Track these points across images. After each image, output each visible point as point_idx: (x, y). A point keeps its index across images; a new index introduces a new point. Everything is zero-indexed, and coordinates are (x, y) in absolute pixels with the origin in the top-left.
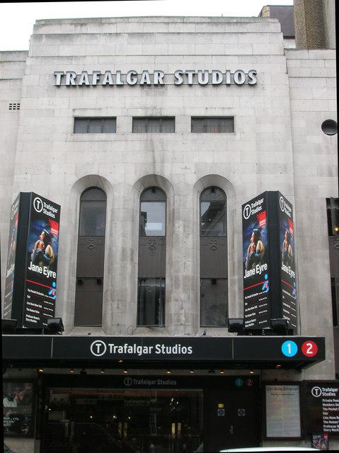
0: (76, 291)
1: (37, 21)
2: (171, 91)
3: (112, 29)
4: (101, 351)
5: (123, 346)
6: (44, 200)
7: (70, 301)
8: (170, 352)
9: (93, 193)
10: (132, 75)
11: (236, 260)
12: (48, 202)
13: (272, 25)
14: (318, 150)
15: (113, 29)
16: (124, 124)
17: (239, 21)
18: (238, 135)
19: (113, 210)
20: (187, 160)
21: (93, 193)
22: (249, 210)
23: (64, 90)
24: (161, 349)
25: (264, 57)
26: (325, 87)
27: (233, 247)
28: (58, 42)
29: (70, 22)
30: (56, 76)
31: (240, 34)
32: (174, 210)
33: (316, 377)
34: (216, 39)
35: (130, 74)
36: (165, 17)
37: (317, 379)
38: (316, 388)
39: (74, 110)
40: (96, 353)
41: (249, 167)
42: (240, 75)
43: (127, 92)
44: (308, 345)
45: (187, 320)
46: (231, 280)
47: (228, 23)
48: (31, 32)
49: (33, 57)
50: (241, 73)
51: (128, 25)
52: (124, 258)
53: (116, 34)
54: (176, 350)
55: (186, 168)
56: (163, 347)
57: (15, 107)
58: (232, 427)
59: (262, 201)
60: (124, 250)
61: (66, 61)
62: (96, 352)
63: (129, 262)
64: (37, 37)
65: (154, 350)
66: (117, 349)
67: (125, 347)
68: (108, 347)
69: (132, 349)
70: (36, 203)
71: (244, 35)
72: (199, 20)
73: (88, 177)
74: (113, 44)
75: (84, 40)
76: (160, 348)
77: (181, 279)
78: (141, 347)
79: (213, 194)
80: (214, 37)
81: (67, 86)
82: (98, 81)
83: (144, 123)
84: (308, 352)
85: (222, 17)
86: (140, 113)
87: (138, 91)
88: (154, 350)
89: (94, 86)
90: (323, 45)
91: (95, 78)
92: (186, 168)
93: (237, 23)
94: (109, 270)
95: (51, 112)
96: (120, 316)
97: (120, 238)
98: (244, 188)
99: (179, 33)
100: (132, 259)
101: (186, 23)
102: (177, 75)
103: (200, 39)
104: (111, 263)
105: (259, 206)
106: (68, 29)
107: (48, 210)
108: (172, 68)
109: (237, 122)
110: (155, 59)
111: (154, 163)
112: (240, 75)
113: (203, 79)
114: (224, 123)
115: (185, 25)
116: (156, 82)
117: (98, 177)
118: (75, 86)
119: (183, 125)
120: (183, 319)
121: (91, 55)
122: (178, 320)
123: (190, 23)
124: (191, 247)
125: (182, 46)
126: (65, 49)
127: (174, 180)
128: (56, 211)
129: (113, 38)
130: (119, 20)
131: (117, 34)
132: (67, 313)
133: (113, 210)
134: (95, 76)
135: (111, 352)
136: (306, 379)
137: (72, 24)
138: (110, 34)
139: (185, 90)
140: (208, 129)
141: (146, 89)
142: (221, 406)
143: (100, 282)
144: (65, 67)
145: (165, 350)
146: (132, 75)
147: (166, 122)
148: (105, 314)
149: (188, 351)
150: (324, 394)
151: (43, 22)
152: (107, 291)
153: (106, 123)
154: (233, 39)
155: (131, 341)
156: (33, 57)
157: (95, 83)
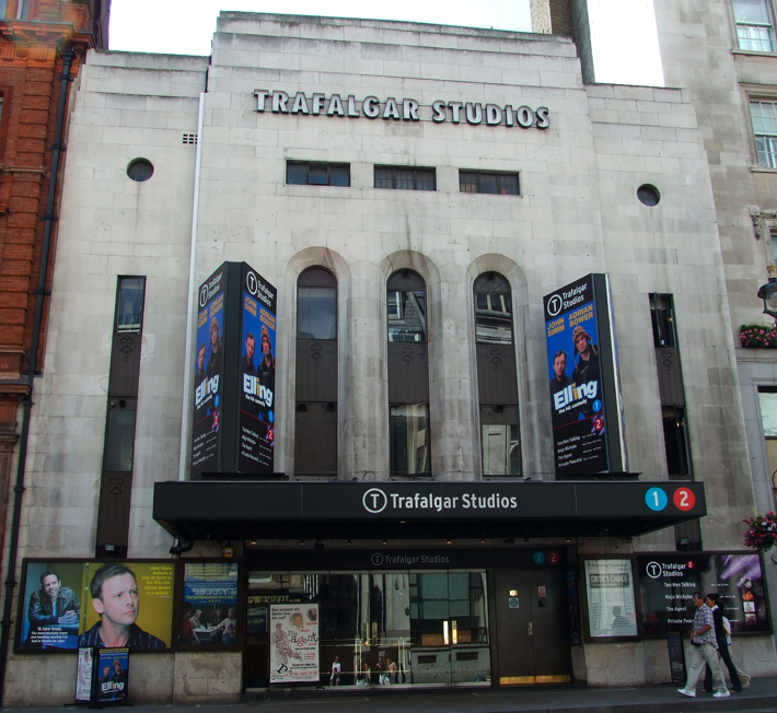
0: (297, 421)
1: (221, 13)
2: (429, 129)
3: (337, 35)
6: (259, 277)
7: (288, 436)
8: (484, 506)
9: (319, 277)
10: (372, 102)
11: (532, 378)
12: (264, 282)
13: (564, 46)
14: (634, 225)
15: (337, 35)
16: (362, 175)
17: (518, 37)
18: (526, 200)
19: (349, 301)
20: (455, 234)
21: (319, 277)
22: (558, 303)
23: (268, 118)
25: (558, 92)
26: (638, 138)
27: (526, 359)
28: (256, 46)
29: (273, 18)
30: (256, 96)
31: (521, 57)
32: (440, 303)
33: (650, 548)
35: (369, 101)
36: (413, 23)
37: (652, 550)
38: (653, 565)
39: (286, 149)
40: (372, 508)
41: (544, 244)
42: (525, 113)
44: (681, 493)
45: (466, 465)
47: (505, 40)
48: (214, 28)
49: (218, 66)
50: (284, 96)
51: (359, 29)
52: (370, 374)
53: (344, 42)
54: (492, 502)
55: (455, 242)
56: (474, 498)
57: (190, 140)
59: (584, 288)
60: (370, 361)
61: (270, 77)
63: (377, 378)
64: (222, 37)
65: (460, 502)
66: (404, 502)
67: (417, 499)
68: (390, 500)
69: (426, 502)
70: (250, 280)
71: (527, 58)
72: (461, 32)
73: (310, 251)
74: (340, 58)
75: (296, 47)
76: (469, 499)
77: (455, 404)
78: (440, 499)
79: (492, 286)
80: (485, 57)
81: (274, 112)
82: (321, 107)
83: (390, 176)
84: (682, 504)
85: (491, 30)
86: (387, 160)
87: (380, 124)
88: (460, 502)
89: (316, 115)
91: (317, 104)
92: (455, 242)
93: (515, 40)
94: (348, 391)
95: (252, 151)
97: (365, 335)
98: (544, 269)
99: (435, 48)
100: (381, 375)
101: (445, 34)
102: (437, 108)
103: (467, 59)
104: (350, 379)
105: (578, 295)
107: (264, 294)
108: (429, 96)
109: (524, 181)
110: (403, 82)
111: (408, 232)
112: (525, 113)
113: (475, 116)
114: (503, 182)
115: (443, 37)
116: (407, 116)
118: (286, 113)
119: (448, 180)
120: (461, 463)
121: (309, 70)
122: (455, 465)
123: (450, 35)
124: (467, 356)
125: (439, 66)
126: (269, 58)
128: (271, 296)
129: (340, 48)
130: (346, 22)
131: (345, 43)
132: (286, 455)
133: (349, 301)
134: (317, 99)
136: (636, 550)
137: (275, 22)
138: (335, 41)
139: (448, 129)
141: (392, 124)
142: (513, 593)
143: (332, 407)
144: (271, 85)
145: (477, 502)
146: (372, 102)
147: (423, 177)
149: (511, 503)
150: (666, 574)
151: (232, 16)
152: (345, 421)
153: (333, 173)
154: (512, 62)
156: (218, 66)
157: (316, 110)
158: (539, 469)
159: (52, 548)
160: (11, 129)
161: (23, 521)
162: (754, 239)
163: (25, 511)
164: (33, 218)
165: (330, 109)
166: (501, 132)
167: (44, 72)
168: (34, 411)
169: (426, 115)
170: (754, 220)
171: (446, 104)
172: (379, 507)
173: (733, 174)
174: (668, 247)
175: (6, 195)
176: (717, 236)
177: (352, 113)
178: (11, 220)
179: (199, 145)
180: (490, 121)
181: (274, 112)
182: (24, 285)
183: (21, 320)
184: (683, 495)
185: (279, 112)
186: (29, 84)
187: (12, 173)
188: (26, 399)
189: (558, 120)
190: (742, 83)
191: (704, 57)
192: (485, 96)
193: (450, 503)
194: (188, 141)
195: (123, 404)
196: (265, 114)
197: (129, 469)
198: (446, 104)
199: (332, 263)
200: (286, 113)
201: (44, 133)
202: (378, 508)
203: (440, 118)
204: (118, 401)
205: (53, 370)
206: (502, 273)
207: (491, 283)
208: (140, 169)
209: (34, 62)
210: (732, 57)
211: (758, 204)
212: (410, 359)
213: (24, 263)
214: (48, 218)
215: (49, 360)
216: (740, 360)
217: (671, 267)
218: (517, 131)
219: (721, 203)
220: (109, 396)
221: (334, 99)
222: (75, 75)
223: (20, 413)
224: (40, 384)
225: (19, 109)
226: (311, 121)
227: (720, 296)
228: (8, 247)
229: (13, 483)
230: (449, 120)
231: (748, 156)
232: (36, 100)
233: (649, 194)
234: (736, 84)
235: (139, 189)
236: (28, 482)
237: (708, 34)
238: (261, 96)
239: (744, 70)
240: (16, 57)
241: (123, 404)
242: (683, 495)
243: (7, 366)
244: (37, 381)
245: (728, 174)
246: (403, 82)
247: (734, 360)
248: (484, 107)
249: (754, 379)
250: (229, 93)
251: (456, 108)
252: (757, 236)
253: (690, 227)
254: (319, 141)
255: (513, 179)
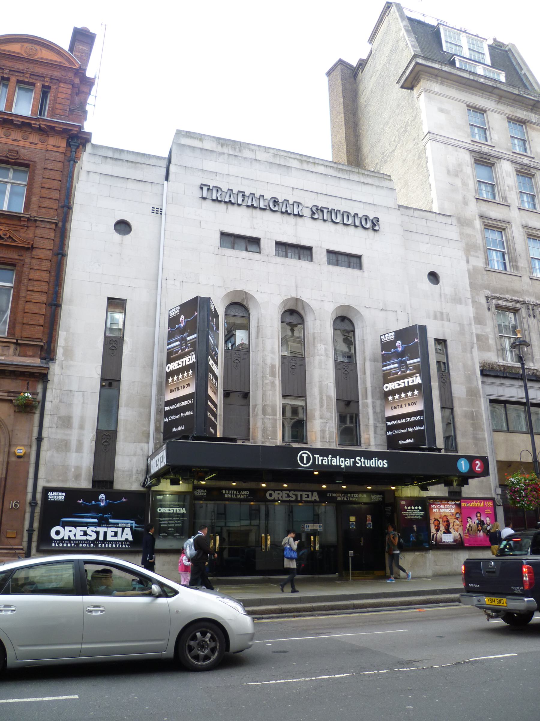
2: (309, 222)
4: (308, 461)
5: (328, 457)
8: (369, 465)
18: (366, 274)
20: (324, 291)
23: (209, 203)
24: (361, 462)
30: (202, 188)
32: (314, 334)
34: (343, 184)
40: (303, 463)
43: (268, 214)
44: (477, 462)
45: (330, 438)
46: (363, 403)
50: (219, 190)
54: (374, 463)
56: (363, 460)
57: (157, 211)
58: (362, 539)
62: (302, 461)
65: (355, 462)
66: (322, 460)
67: (330, 458)
68: (314, 458)
76: (360, 460)
78: (343, 459)
82: (243, 200)
83: (284, 248)
87: (278, 216)
88: (355, 462)
89: (239, 205)
90: (31, 115)
92: (324, 296)
96: (323, 429)
102: (314, 209)
104: (501, 385)
106: (208, 145)
108: (309, 201)
110: (293, 191)
114: (353, 260)
117: (246, 294)
119: (320, 255)
126: (210, 164)
127: (314, 304)
135: (317, 463)
139: (320, 223)
140: (236, 246)
143: (246, 395)
146: (275, 201)
147: (304, 251)
148: (254, 429)
149: (384, 464)
155: (334, 453)
157: (240, 202)
158: (372, 442)
159: (63, 481)
160: (34, 190)
161: (41, 461)
162: (487, 310)
163: (43, 454)
164: (50, 253)
165: (253, 203)
166: (352, 229)
167: (58, 154)
168: (49, 386)
169: (307, 213)
170: (487, 299)
171: (319, 208)
172: (308, 463)
173: (475, 269)
174: (444, 311)
175: (31, 235)
176: (471, 307)
177: (262, 206)
178: (35, 252)
179: (163, 215)
180: (345, 222)
181: (213, 200)
182: (43, 298)
183: (42, 322)
184: (478, 464)
185: (217, 200)
186: (48, 162)
187: (36, 221)
188: (42, 377)
189: (383, 224)
190: (481, 217)
191: (460, 198)
192: (342, 206)
193: (349, 462)
194: (159, 210)
195: (110, 385)
196: (207, 201)
197: (113, 428)
198: (319, 208)
199: (247, 302)
200: (220, 201)
201: (58, 195)
202: (307, 464)
203: (316, 216)
204: (107, 383)
205: (63, 358)
206: (350, 318)
207: (342, 323)
208: (123, 227)
209: (52, 147)
210: (475, 200)
211: (489, 290)
212: (294, 369)
213: (44, 283)
214: (60, 255)
215: (60, 352)
216: (483, 382)
217: (446, 323)
218: (360, 230)
219: (473, 286)
220: (101, 379)
221: (251, 196)
222: (79, 159)
223: (40, 389)
224: (56, 370)
225: (41, 177)
226: (236, 207)
227: (473, 343)
228: (33, 271)
229: (35, 434)
230: (321, 218)
231: (484, 260)
232: (53, 173)
233: (434, 277)
234: (477, 217)
235: (122, 240)
236: (45, 434)
237: (463, 184)
238: (205, 188)
239: (482, 209)
240: (21, 139)
241: (110, 385)
242: (478, 464)
243: (31, 354)
244: (51, 365)
245: (473, 269)
246: (293, 191)
247: (480, 383)
248: (341, 213)
249: (487, 395)
250: (184, 184)
251: (325, 211)
252: (489, 309)
253: (456, 300)
254: (241, 222)
255: (358, 260)
